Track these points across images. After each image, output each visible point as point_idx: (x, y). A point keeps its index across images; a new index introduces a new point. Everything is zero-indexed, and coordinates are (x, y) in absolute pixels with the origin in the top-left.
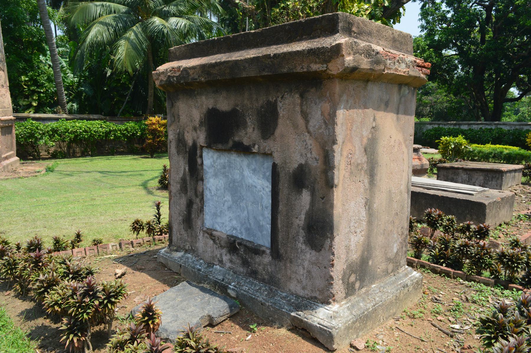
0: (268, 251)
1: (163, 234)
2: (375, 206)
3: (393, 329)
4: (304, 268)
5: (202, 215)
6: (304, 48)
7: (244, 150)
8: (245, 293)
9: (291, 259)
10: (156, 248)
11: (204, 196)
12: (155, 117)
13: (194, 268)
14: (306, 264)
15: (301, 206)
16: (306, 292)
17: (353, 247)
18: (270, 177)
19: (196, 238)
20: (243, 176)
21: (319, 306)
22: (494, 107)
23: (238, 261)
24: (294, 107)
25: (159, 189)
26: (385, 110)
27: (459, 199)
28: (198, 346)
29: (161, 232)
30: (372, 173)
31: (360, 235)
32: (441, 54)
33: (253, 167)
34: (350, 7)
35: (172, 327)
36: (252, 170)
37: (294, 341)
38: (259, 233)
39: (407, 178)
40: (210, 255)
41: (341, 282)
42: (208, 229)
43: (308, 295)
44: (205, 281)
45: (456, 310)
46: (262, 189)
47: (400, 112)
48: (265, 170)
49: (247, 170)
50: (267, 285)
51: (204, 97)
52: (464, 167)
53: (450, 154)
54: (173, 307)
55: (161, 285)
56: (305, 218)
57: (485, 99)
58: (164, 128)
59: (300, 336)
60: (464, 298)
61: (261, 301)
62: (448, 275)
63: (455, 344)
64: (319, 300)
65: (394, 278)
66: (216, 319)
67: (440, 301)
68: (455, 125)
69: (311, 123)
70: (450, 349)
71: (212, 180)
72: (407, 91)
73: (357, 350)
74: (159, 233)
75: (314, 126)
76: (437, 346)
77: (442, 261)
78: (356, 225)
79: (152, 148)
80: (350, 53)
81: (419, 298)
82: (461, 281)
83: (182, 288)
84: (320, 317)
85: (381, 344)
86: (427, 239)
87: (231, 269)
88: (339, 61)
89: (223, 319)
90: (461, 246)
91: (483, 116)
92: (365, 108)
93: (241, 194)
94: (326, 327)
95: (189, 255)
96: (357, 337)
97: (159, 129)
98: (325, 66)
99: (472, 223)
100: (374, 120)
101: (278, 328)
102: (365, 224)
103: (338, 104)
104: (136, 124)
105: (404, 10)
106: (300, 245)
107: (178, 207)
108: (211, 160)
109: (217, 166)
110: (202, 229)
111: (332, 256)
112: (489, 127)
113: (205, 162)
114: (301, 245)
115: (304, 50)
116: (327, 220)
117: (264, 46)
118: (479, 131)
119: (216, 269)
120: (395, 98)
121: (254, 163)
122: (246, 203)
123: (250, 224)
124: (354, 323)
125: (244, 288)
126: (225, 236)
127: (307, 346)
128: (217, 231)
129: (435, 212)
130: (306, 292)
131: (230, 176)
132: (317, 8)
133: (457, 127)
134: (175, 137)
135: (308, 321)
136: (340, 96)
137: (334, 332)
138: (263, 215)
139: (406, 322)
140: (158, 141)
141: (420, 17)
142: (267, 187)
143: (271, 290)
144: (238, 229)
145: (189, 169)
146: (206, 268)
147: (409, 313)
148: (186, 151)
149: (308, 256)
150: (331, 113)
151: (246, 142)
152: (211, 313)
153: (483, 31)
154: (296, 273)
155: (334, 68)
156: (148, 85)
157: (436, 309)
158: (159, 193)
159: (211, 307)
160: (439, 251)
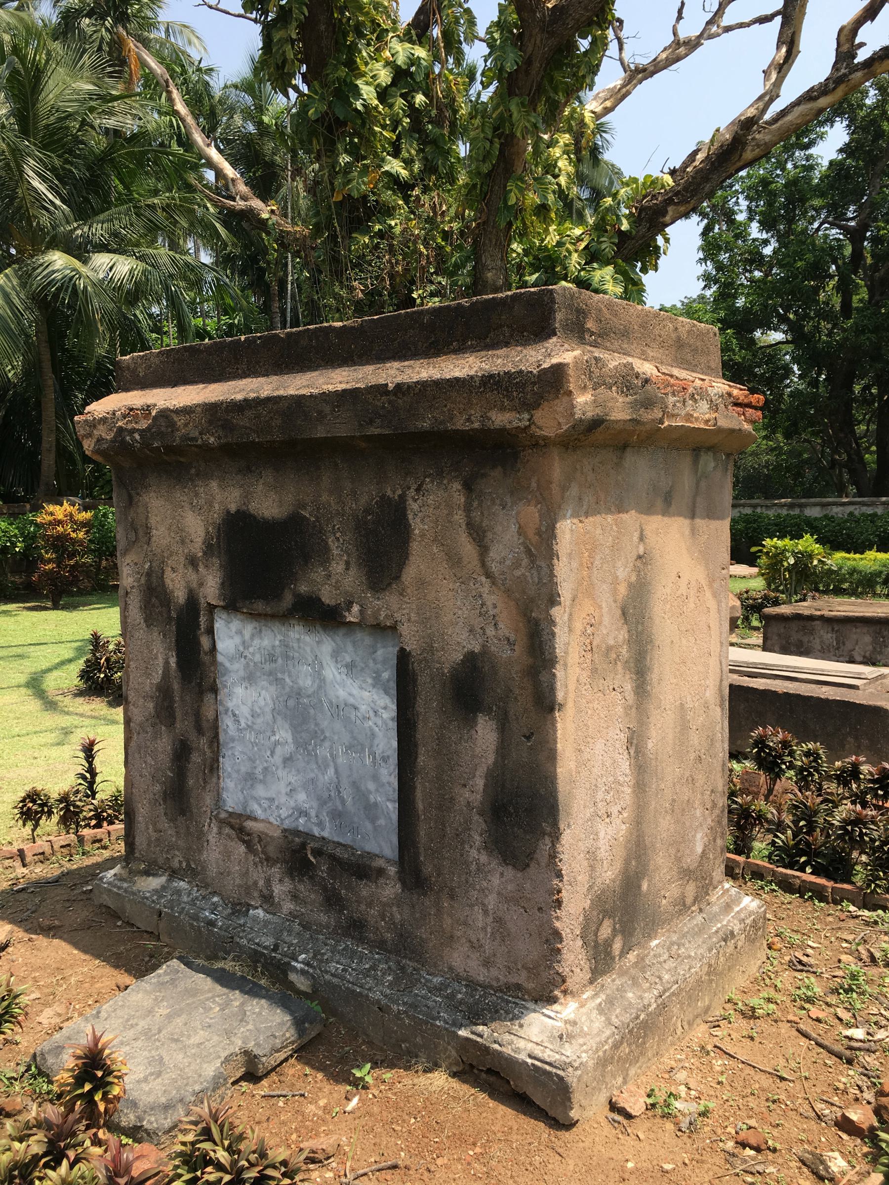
0: (392, 870)
1: (105, 824)
2: (650, 745)
3: (708, 1053)
4: (486, 912)
5: (214, 780)
6: (472, 373)
7: (323, 616)
8: (335, 980)
9: (452, 889)
10: (88, 861)
11: (220, 730)
12: (62, 505)
13: (196, 917)
14: (491, 901)
15: (474, 756)
16: (494, 972)
17: (603, 853)
18: (393, 685)
19: (199, 839)
20: (323, 680)
21: (527, 1009)
22: (879, 461)
23: (313, 896)
24: (450, 514)
25: (80, 693)
26: (665, 513)
27: (827, 701)
28: (237, 1161)
29: (99, 819)
30: (640, 668)
31: (619, 821)
32: (753, 341)
33: (348, 659)
34: (539, 233)
35: (150, 1092)
36: (346, 666)
37: (471, 1105)
38: (369, 826)
39: (718, 671)
40: (238, 881)
41: (579, 943)
42: (231, 814)
43: (498, 980)
44: (228, 953)
45: (852, 990)
46: (372, 714)
47: (698, 511)
48: (379, 666)
49: (332, 665)
50: (393, 957)
51: (214, 484)
52: (826, 613)
53: (785, 579)
54: (147, 1034)
55: (108, 970)
56: (485, 785)
57: (857, 444)
58: (87, 532)
59: (482, 1090)
60: (865, 955)
61: (378, 1002)
62: (819, 894)
63: (860, 1083)
64: (528, 992)
65: (699, 918)
66: (264, 1059)
67: (810, 966)
68: (791, 506)
69: (497, 552)
70: (851, 1096)
71: (239, 691)
72: (712, 464)
73: (629, 1116)
74: (93, 822)
75: (502, 562)
76: (819, 1091)
77: (803, 859)
78: (608, 798)
79: (55, 585)
80: (585, 386)
81: (759, 963)
82: (852, 908)
83: (167, 978)
84: (532, 1037)
85: (683, 1095)
86: (761, 804)
87: (295, 917)
88: (560, 405)
89: (281, 1056)
90: (846, 822)
91: (855, 483)
92: (619, 512)
93: (317, 725)
94: (550, 1064)
95: (182, 883)
96: (625, 1082)
97: (73, 535)
98: (526, 416)
99: (862, 759)
100: (642, 538)
101: (425, 1071)
102: (629, 791)
103: (560, 507)
104: (11, 524)
105: (667, 240)
106: (474, 853)
107: (149, 759)
108: (237, 640)
109: (253, 654)
110: (216, 817)
111: (556, 882)
112: (869, 511)
113: (220, 646)
114: (477, 855)
115: (472, 377)
116: (542, 791)
117: (368, 363)
118: (847, 521)
119: (255, 919)
120: (686, 481)
121: (350, 648)
122: (331, 748)
123: (343, 802)
124: (616, 1046)
125: (333, 966)
126: (277, 834)
127: (503, 1116)
128: (255, 819)
129: (776, 737)
130: (494, 972)
131: (287, 680)
132: (462, 233)
133: (797, 511)
134: (139, 580)
135: (504, 1049)
136: (564, 489)
137: (571, 1077)
138: (375, 778)
139: (737, 1030)
140: (72, 567)
141: (701, 255)
142: (385, 708)
143: (403, 969)
144: (313, 813)
145: (178, 663)
146: (228, 917)
147: (740, 1004)
148: (170, 618)
149: (496, 881)
150: (544, 529)
151: (328, 596)
152: (251, 1045)
153: (845, 288)
154: (465, 924)
155: (549, 422)
156: (40, 422)
157: (804, 990)
158: (84, 706)
159: (250, 1027)
160: (795, 836)
